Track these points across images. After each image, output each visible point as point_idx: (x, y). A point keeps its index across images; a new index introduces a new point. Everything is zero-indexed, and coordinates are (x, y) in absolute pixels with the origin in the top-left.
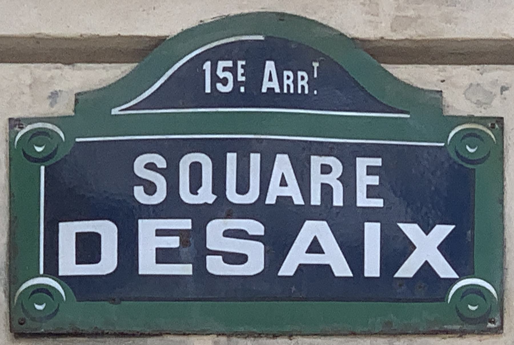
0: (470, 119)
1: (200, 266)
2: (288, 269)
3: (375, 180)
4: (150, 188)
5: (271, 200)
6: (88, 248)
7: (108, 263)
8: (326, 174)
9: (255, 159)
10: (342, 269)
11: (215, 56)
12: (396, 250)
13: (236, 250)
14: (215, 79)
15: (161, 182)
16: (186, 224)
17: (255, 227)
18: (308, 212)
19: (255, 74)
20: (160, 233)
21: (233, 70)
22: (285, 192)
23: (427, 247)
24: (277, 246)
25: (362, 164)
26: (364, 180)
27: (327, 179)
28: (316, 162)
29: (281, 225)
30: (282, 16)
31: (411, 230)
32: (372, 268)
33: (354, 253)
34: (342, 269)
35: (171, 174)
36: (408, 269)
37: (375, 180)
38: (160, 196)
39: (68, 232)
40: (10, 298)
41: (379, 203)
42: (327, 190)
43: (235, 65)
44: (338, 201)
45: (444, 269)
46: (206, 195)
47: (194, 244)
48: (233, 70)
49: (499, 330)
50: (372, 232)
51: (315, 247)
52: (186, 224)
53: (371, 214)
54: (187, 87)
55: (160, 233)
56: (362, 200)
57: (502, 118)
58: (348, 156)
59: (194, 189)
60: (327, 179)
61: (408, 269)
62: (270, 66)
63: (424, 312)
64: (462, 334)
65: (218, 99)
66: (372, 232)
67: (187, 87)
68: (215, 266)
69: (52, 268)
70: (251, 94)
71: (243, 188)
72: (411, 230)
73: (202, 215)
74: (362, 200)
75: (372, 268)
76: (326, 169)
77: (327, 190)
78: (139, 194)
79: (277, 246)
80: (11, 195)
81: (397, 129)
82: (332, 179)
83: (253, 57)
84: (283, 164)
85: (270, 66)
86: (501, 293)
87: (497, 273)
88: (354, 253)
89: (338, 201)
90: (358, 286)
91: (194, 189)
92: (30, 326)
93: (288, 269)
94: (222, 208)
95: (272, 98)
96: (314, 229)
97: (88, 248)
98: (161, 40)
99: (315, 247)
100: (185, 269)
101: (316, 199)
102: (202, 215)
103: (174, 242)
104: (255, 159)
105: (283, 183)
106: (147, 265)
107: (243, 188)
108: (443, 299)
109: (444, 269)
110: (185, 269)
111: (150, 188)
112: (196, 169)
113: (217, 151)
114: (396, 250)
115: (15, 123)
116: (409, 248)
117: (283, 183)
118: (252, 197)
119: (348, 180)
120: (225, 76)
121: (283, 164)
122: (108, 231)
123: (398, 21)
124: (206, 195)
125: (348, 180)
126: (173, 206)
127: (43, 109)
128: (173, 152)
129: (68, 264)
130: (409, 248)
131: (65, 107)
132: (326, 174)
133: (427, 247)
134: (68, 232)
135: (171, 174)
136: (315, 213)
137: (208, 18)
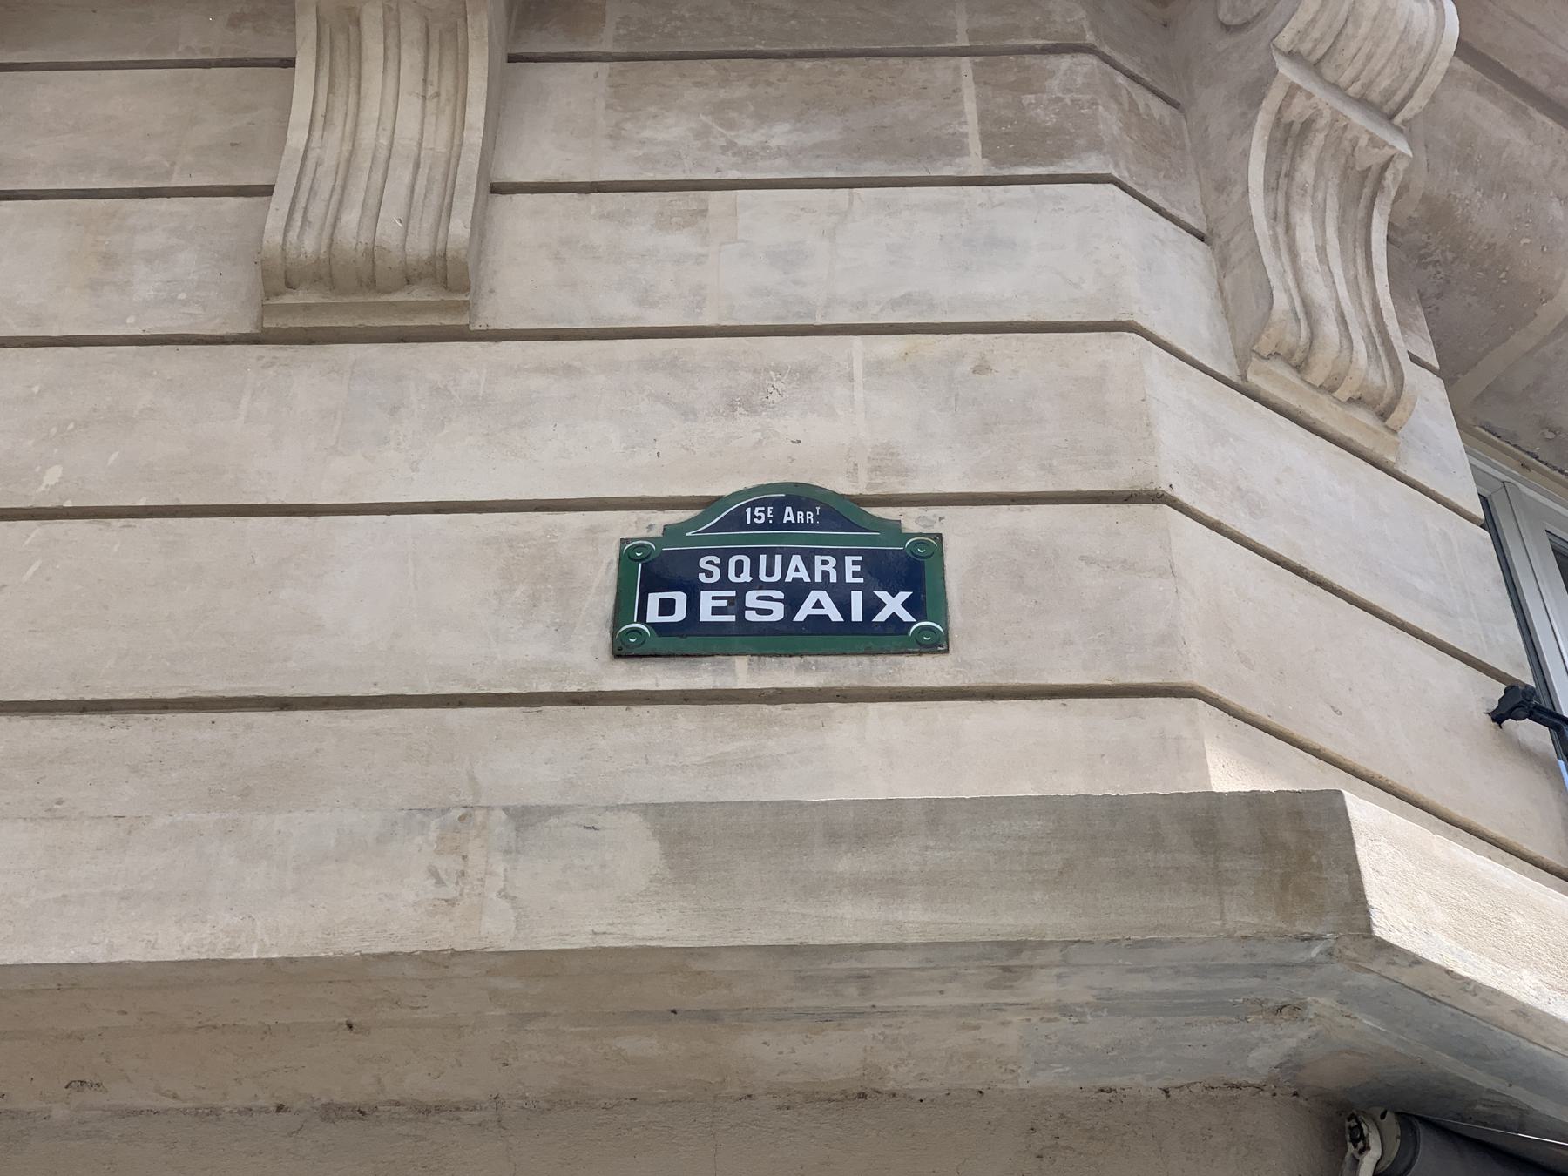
0: (920, 534)
1: (740, 616)
2: (800, 617)
3: (858, 568)
4: (709, 574)
5: (788, 579)
6: (667, 607)
7: (680, 614)
8: (825, 566)
9: (778, 558)
10: (836, 617)
11: (753, 505)
12: (873, 606)
13: (765, 607)
14: (753, 516)
15: (717, 572)
16: (733, 593)
17: (779, 595)
18: (813, 586)
19: (779, 513)
20: (714, 598)
21: (765, 512)
22: (798, 575)
23: (894, 605)
24: (793, 604)
25: (849, 560)
26: (850, 568)
27: (825, 568)
28: (818, 559)
29: (795, 594)
30: (796, 484)
31: (883, 595)
32: (857, 615)
33: (845, 608)
34: (836, 617)
35: (723, 568)
36: (882, 617)
37: (858, 568)
38: (716, 578)
39: (654, 599)
40: (613, 636)
41: (861, 580)
42: (826, 574)
43: (1405, 130)
44: (833, 579)
45: (906, 617)
46: (746, 577)
47: (738, 605)
48: (765, 512)
49: (946, 651)
50: (857, 598)
51: (818, 605)
52: (733, 593)
53: (856, 587)
54: (736, 521)
55: (714, 598)
56: (849, 579)
57: (940, 535)
58: (840, 557)
59: (738, 575)
60: (825, 568)
61: (882, 617)
62: (789, 509)
63: (896, 641)
64: (920, 654)
65: (754, 526)
66: (857, 598)
67: (736, 521)
68: (750, 616)
69: (642, 617)
70: (777, 523)
71: (770, 572)
72: (883, 595)
73: (742, 589)
74: (849, 579)
75: (857, 615)
76: (825, 563)
77: (826, 574)
78: (702, 577)
79: (793, 604)
80: (619, 579)
81: (873, 540)
82: (830, 568)
83: (779, 506)
84: (796, 560)
85: (789, 509)
86: (946, 630)
87: (943, 618)
88: (845, 608)
89: (833, 579)
90: (847, 626)
91: (738, 575)
92: (625, 651)
93: (800, 617)
94: (756, 584)
95: (789, 525)
96: (822, 595)
97: (667, 607)
98: (720, 498)
99: (818, 605)
100: (732, 618)
101: (818, 579)
102: (742, 589)
103: (724, 603)
104: (778, 558)
105: (797, 570)
106: (705, 615)
107: (770, 572)
108: (906, 633)
109: (906, 617)
110: (732, 618)
111: (709, 574)
112: (739, 565)
113: (754, 556)
114: (873, 606)
115: (624, 541)
116: (881, 605)
117: (797, 569)
118: (777, 577)
119: (840, 568)
120: (761, 515)
121: (796, 560)
122: (680, 599)
123: (870, 486)
124: (746, 577)
125: (840, 568)
126: (724, 583)
127: (644, 533)
128: (725, 555)
129: (653, 615)
130: (881, 605)
131: (657, 532)
132: (825, 566)
133: (894, 605)
134: (654, 599)
135: (723, 568)
136: (818, 587)
137: (749, 486)
